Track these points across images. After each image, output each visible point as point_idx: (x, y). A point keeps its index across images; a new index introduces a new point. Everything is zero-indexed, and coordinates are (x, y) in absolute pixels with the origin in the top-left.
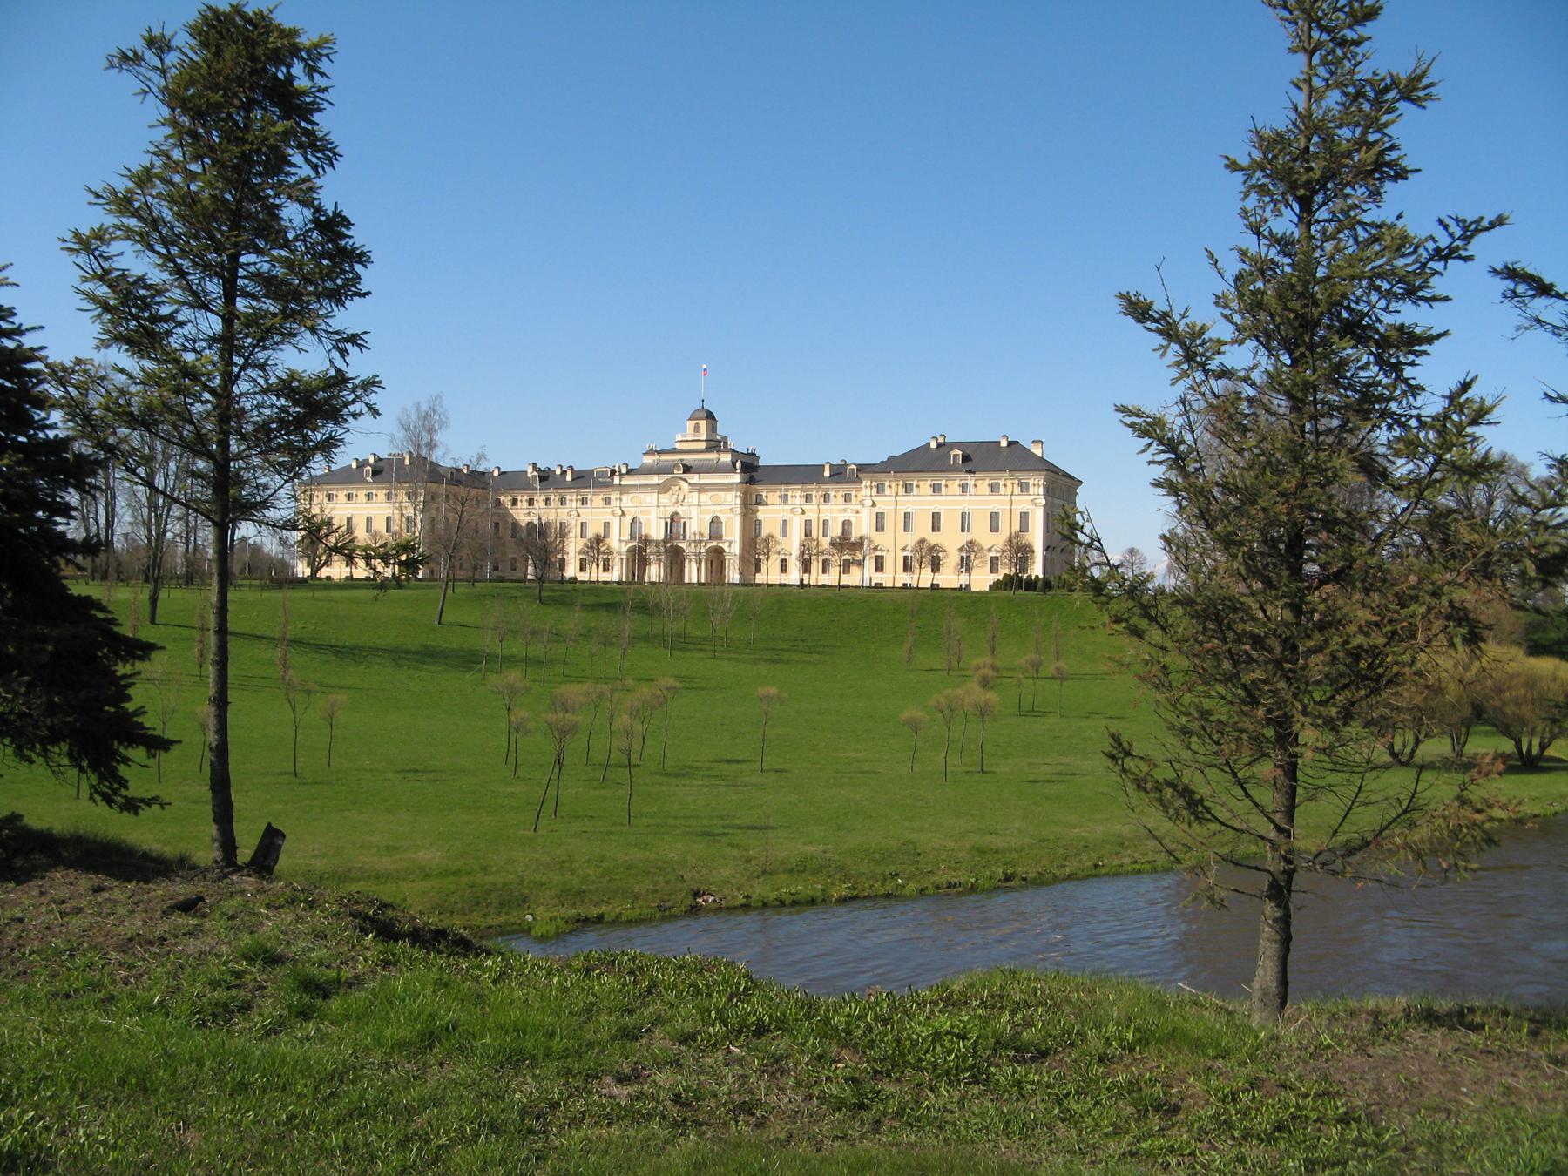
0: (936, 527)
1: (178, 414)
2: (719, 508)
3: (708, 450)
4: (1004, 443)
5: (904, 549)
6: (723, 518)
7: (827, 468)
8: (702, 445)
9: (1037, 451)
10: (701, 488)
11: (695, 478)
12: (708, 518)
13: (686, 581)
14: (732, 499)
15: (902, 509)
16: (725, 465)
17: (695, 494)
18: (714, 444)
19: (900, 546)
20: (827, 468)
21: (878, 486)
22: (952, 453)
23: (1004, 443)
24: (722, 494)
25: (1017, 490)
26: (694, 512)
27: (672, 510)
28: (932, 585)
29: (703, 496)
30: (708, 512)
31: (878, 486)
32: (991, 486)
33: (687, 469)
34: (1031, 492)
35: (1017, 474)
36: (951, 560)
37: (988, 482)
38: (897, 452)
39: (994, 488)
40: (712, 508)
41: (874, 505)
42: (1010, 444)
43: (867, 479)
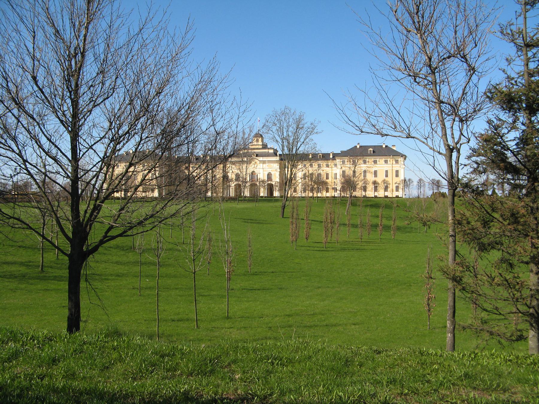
0: (387, 176)
1: (169, 142)
2: (271, 169)
3: (263, 148)
4: (384, 146)
5: (396, 183)
6: (272, 173)
7: (331, 154)
8: (261, 147)
9: (394, 148)
10: (264, 162)
11: (261, 159)
12: (266, 174)
13: (274, 195)
14: (276, 166)
15: (395, 169)
16: (271, 153)
17: (261, 165)
18: (265, 146)
19: (394, 182)
20: (331, 154)
21: (342, 161)
22: (369, 150)
23: (384, 146)
24: (272, 164)
25: (394, 162)
26: (261, 171)
27: (252, 170)
28: (375, 196)
29: (264, 165)
30: (266, 171)
31: (342, 161)
32: (364, 161)
33: (257, 156)
34: (399, 163)
35: (394, 157)
36: (370, 187)
37: (384, 160)
38: (345, 149)
39: (386, 162)
40: (268, 169)
41: (341, 168)
42: (386, 146)
43: (338, 159)
